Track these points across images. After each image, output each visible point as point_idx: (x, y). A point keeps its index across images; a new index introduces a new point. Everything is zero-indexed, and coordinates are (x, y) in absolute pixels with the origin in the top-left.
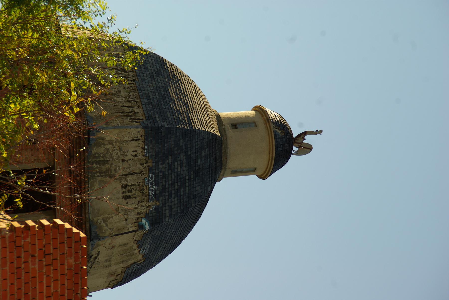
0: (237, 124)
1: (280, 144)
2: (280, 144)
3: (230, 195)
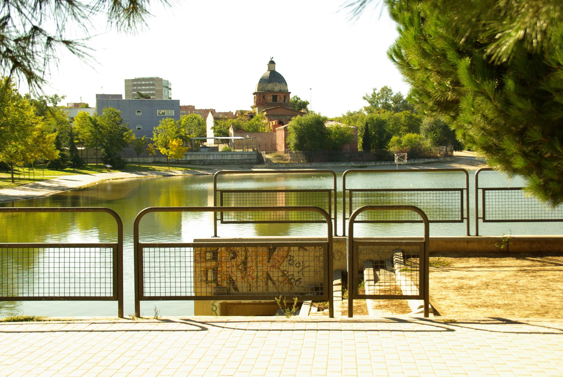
1: (272, 62)
2: (272, 62)
3: (278, 69)
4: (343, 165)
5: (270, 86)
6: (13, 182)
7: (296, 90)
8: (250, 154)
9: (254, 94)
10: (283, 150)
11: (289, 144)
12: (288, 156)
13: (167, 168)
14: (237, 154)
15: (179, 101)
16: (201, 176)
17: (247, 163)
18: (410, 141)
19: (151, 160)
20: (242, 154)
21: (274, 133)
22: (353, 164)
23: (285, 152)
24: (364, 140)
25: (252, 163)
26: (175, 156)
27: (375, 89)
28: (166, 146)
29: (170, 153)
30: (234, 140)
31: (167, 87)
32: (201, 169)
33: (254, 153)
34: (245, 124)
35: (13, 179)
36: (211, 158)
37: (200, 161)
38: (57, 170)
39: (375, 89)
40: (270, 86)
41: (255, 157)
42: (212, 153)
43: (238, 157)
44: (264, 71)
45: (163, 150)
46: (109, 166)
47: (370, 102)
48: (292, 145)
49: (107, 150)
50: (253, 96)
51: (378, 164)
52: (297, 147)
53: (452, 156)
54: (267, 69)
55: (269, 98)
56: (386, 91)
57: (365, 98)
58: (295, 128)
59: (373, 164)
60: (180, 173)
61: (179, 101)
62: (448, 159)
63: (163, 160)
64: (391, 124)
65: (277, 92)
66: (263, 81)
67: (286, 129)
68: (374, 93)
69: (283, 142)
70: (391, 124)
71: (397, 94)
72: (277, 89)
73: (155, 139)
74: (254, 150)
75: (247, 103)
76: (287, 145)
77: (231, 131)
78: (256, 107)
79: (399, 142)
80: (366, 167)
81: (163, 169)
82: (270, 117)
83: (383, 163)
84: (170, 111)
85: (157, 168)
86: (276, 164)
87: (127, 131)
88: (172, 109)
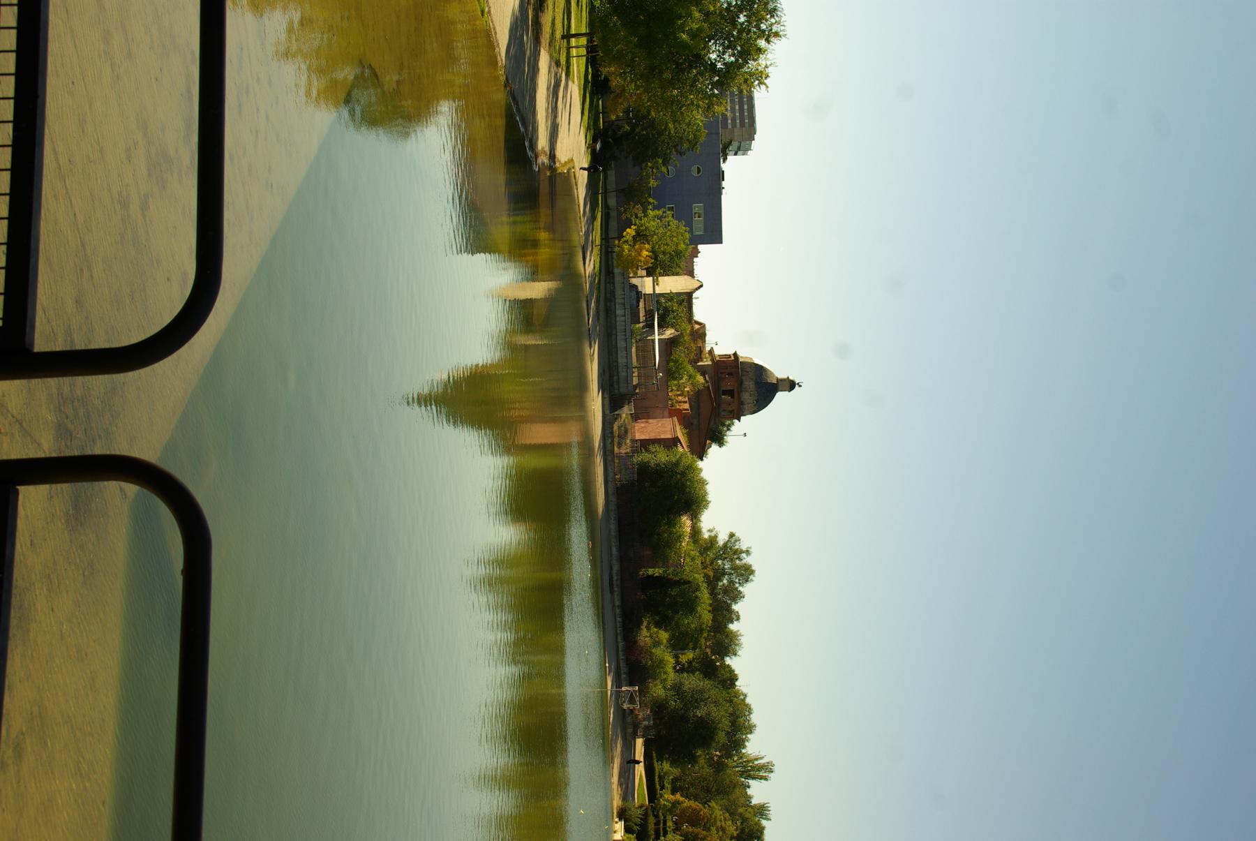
0: (782, 380)
1: (791, 385)
2: (791, 385)
3: (780, 396)
4: (614, 550)
5: (749, 384)
6: (563, 37)
7: (746, 432)
8: (628, 380)
9: (735, 354)
10: (638, 436)
11: (647, 450)
12: (625, 449)
13: (598, 242)
14: (627, 350)
15: (718, 240)
16: (584, 305)
17: (611, 376)
18: (661, 663)
19: (612, 202)
20: (628, 366)
21: (666, 413)
22: (616, 568)
23: (634, 441)
24: (660, 578)
25: (611, 385)
26: (620, 254)
27: (748, 552)
28: (641, 236)
29: (626, 247)
30: (653, 341)
31: (739, 149)
32: (598, 301)
33: (631, 388)
34: (680, 354)
35: (567, 36)
36: (619, 312)
37: (613, 293)
38: (563, 674)
39: (748, 552)
40: (749, 384)
41: (623, 390)
42: (628, 311)
43: (622, 361)
44: (779, 371)
45: (630, 232)
46: (598, 147)
47: (725, 545)
48: (645, 457)
49: (627, 135)
50: (731, 352)
51: (618, 611)
52: (643, 468)
53: (635, 735)
54: (780, 376)
55: (728, 384)
56: (746, 573)
57: (732, 535)
58: (677, 464)
59: (617, 603)
60: (589, 269)
61: (718, 240)
62: (630, 730)
63: (613, 225)
64: (689, 622)
65: (739, 398)
66: (759, 370)
67: (675, 441)
68: (742, 552)
69: (652, 436)
70: (689, 622)
71: (740, 592)
72: (746, 397)
73: (651, 213)
74: (635, 387)
75: (720, 342)
76: (645, 444)
77: (669, 333)
78: (712, 360)
79: (657, 644)
80: (612, 592)
81: (597, 236)
82: (696, 398)
83: (619, 619)
84: (702, 226)
85: (598, 223)
86: (612, 433)
87: (664, 164)
88: (705, 231)
